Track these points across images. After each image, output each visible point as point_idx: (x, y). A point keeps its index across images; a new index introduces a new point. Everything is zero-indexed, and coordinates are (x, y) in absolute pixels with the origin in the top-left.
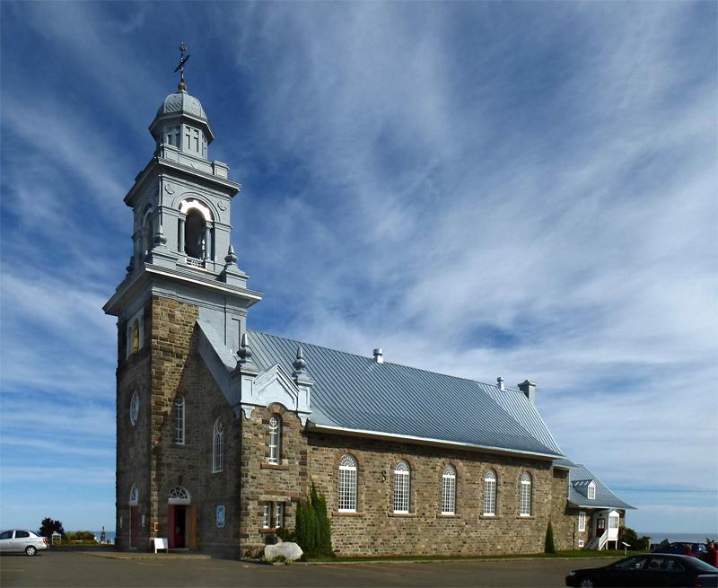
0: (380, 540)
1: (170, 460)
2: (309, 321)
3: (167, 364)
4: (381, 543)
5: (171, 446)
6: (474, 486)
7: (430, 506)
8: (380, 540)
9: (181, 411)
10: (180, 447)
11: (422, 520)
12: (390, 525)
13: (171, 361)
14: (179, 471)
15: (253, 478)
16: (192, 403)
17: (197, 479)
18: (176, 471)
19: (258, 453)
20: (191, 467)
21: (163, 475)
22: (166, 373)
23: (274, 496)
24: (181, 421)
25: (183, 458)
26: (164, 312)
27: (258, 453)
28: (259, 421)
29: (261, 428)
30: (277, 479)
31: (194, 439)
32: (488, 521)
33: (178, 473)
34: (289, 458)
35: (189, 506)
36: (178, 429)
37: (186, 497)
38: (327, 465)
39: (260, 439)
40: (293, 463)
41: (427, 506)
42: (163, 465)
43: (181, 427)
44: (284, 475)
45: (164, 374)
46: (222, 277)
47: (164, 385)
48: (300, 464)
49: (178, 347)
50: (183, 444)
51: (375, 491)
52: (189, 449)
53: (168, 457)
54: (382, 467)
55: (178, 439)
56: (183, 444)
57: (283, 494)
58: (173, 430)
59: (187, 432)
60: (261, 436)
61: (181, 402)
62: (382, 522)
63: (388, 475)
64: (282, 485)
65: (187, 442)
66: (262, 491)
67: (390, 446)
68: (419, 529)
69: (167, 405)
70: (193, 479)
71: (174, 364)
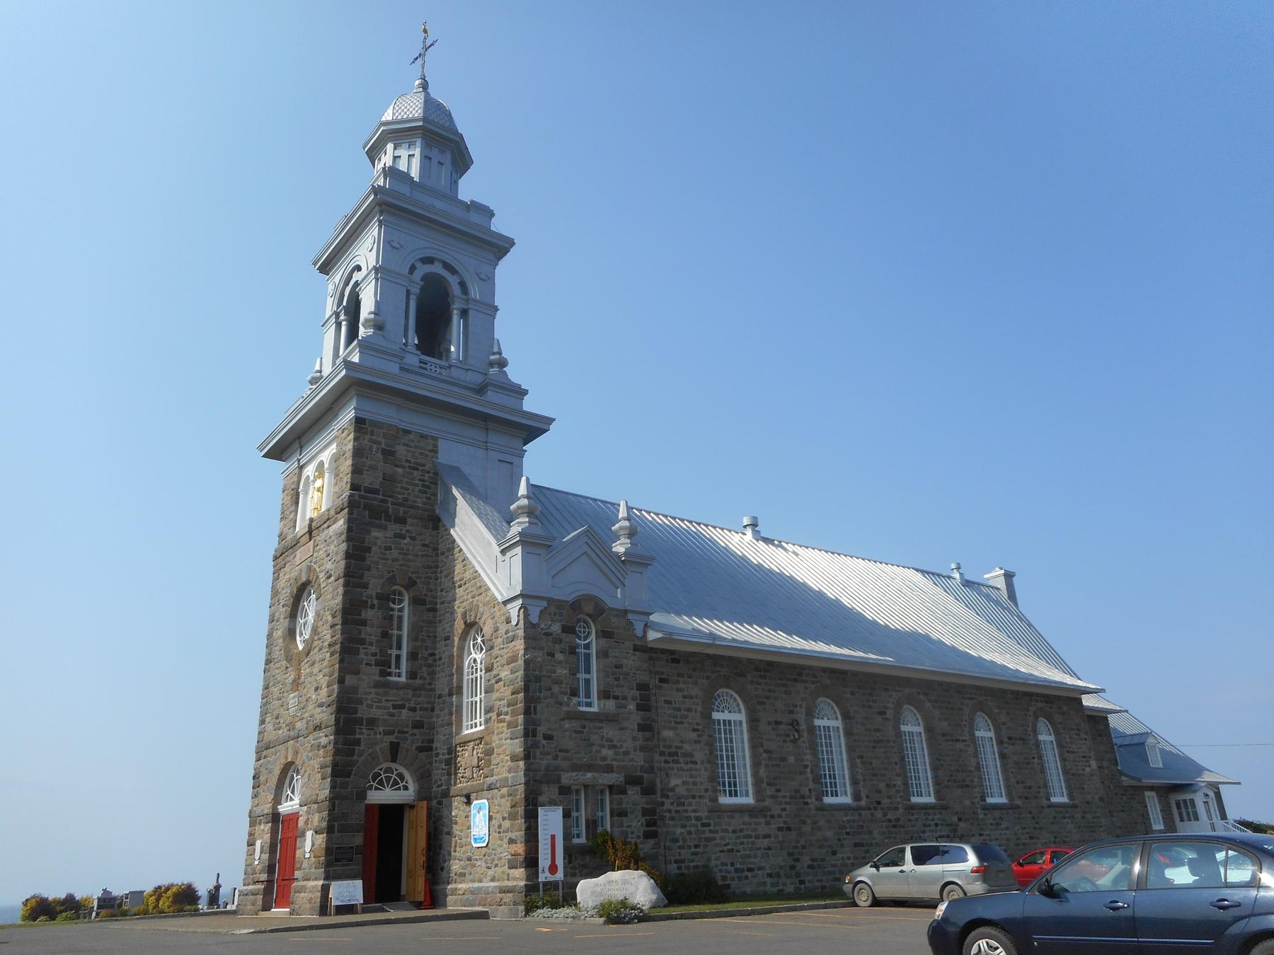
0: (806, 860)
1: (375, 713)
2: (439, 884)
3: (375, 533)
4: (810, 867)
5: (377, 685)
6: (960, 746)
7: (888, 786)
8: (806, 860)
9: (400, 618)
10: (397, 686)
11: (879, 814)
12: (819, 829)
13: (385, 528)
14: (391, 733)
15: (548, 737)
16: (423, 603)
17: (430, 749)
18: (386, 733)
19: (556, 689)
20: (418, 725)
21: (358, 742)
22: (374, 549)
23: (589, 775)
24: (400, 638)
25: (402, 707)
26: (375, 447)
27: (556, 689)
28: (556, 628)
29: (560, 641)
30: (594, 738)
31: (424, 669)
32: (997, 814)
33: (392, 738)
34: (616, 698)
35: (412, 807)
36: (394, 652)
37: (406, 788)
38: (689, 710)
39: (560, 662)
40: (625, 707)
41: (882, 786)
42: (359, 722)
43: (399, 647)
44: (610, 732)
45: (369, 550)
46: (896, 764)
47: (369, 569)
48: (639, 708)
49: (399, 505)
50: (403, 679)
51: (784, 759)
52: (415, 689)
53: (370, 706)
54: (791, 712)
55: (393, 670)
56: (403, 679)
57: (609, 769)
58: (383, 652)
59: (413, 656)
60: (559, 657)
61: (401, 601)
62: (804, 822)
63: (803, 727)
64: (605, 752)
65: (412, 675)
66: (565, 764)
67: (800, 674)
68: (875, 833)
69: (372, 607)
70: (420, 749)
71: (390, 534)
